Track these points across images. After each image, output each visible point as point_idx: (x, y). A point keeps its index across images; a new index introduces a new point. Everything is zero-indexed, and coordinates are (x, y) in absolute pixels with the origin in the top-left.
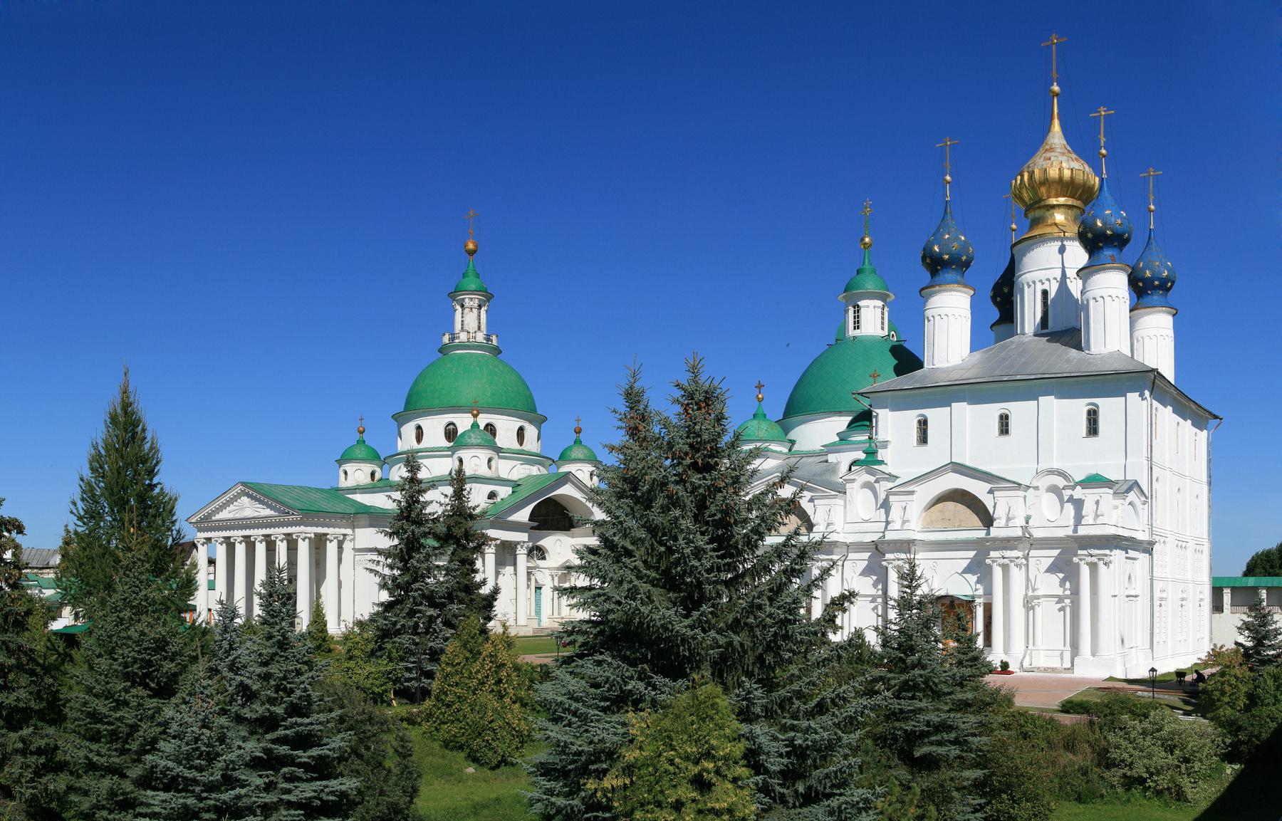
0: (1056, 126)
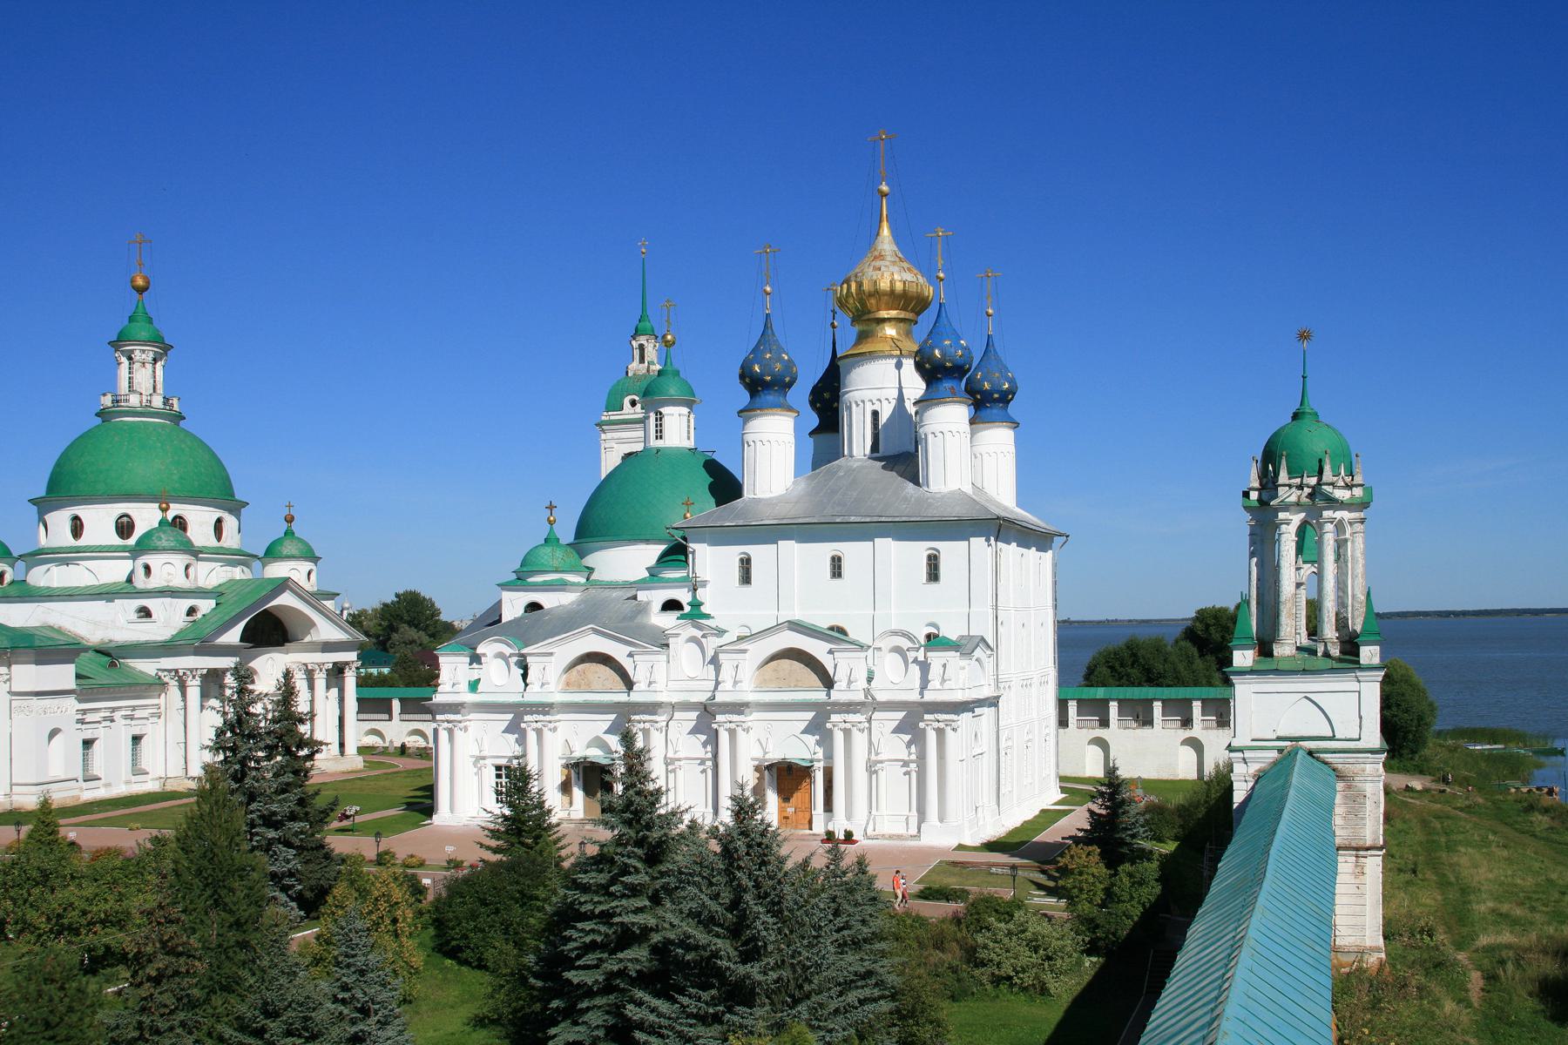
0: (886, 231)
